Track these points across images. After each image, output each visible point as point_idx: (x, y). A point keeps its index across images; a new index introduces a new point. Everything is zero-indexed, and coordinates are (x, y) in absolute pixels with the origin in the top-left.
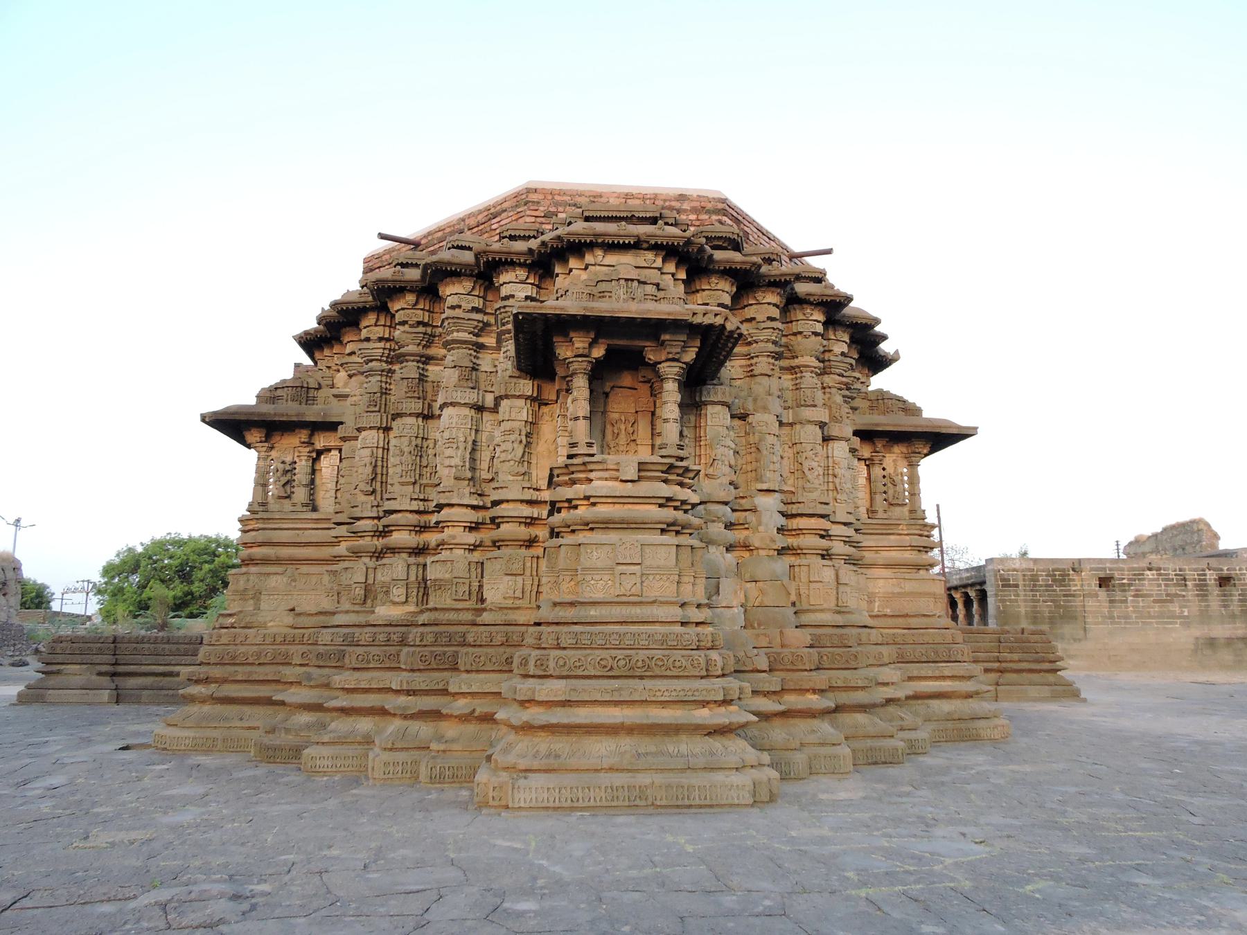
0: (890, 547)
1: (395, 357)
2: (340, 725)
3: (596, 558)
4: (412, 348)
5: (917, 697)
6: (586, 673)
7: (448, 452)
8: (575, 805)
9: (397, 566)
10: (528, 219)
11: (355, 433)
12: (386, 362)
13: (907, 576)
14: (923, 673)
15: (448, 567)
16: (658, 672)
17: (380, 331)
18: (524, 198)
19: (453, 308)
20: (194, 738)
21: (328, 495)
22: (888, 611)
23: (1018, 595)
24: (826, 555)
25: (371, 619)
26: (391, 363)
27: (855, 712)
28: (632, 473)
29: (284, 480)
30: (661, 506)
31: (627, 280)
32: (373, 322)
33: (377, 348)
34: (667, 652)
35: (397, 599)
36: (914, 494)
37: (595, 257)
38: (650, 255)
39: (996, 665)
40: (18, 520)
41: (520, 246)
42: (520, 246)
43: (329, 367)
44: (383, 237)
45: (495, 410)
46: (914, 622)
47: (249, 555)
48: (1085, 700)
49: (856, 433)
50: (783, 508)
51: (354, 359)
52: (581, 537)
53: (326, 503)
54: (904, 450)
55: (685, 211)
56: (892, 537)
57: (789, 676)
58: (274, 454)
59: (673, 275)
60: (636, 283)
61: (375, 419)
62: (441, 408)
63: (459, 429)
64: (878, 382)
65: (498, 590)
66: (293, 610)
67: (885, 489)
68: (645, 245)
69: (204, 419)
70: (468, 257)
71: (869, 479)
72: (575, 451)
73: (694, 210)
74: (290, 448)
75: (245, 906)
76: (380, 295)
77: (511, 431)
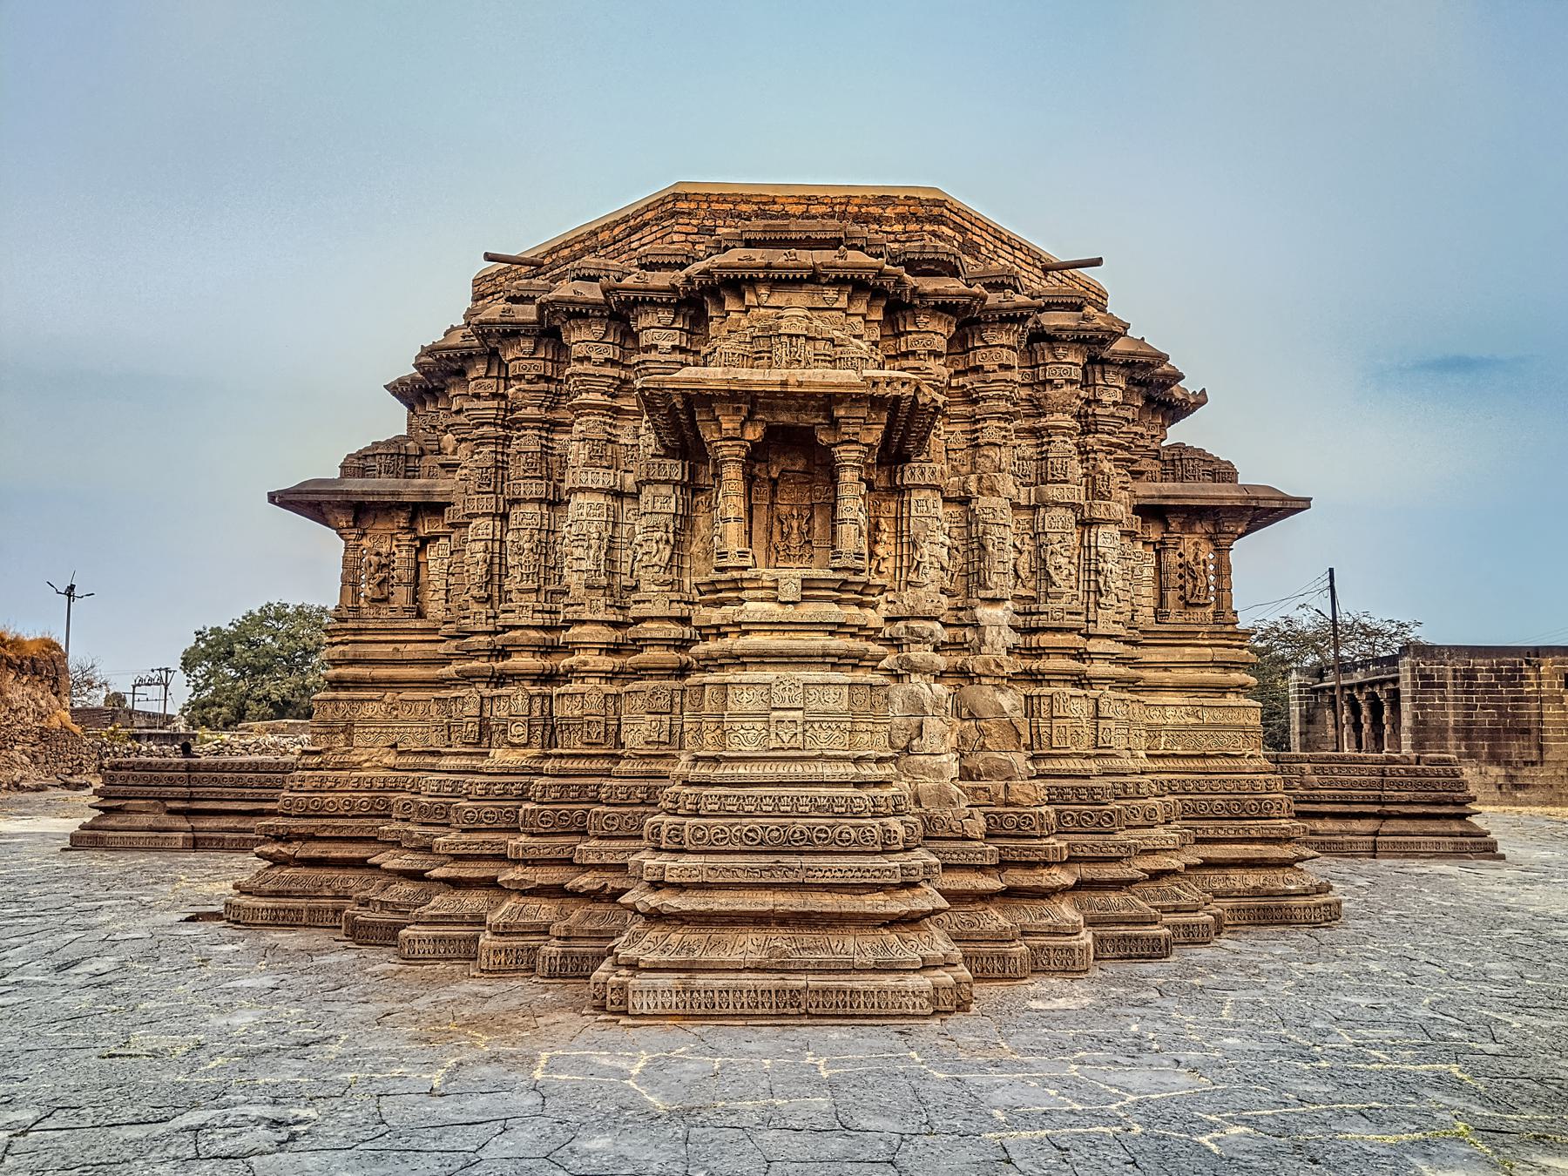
0: (1183, 665)
1: (510, 423)
2: (442, 903)
3: (744, 701)
4: (530, 412)
5: (1208, 864)
7: (578, 552)
8: (711, 1012)
9: (517, 698)
10: (676, 238)
11: (466, 520)
12: (503, 426)
13: (1205, 702)
15: (580, 700)
17: (491, 385)
18: (669, 207)
19: (580, 360)
21: (436, 597)
23: (1445, 699)
24: (1081, 680)
25: (485, 764)
26: (508, 427)
27: (1107, 889)
28: (791, 591)
29: (380, 576)
30: (831, 633)
31: (790, 336)
32: (482, 373)
33: (489, 408)
34: (831, 821)
35: (516, 740)
36: (1223, 590)
37: (758, 296)
38: (831, 293)
39: (1376, 809)
40: (72, 587)
41: (660, 279)
42: (660, 279)
43: (434, 427)
44: (489, 257)
45: (636, 496)
47: (337, 676)
48: (1502, 857)
49: (1137, 510)
50: (1020, 621)
51: (462, 418)
52: (730, 676)
53: (435, 608)
55: (888, 219)
56: (1188, 650)
57: (1011, 843)
58: (366, 542)
59: (864, 316)
60: (802, 340)
61: (487, 503)
62: (572, 491)
63: (591, 522)
64: (1178, 433)
65: (639, 732)
66: (394, 746)
68: (824, 280)
69: (272, 498)
70: (593, 293)
71: (1159, 570)
72: (723, 563)
73: (902, 218)
74: (387, 541)
75: (284, 1135)
76: (487, 343)
77: (655, 527)
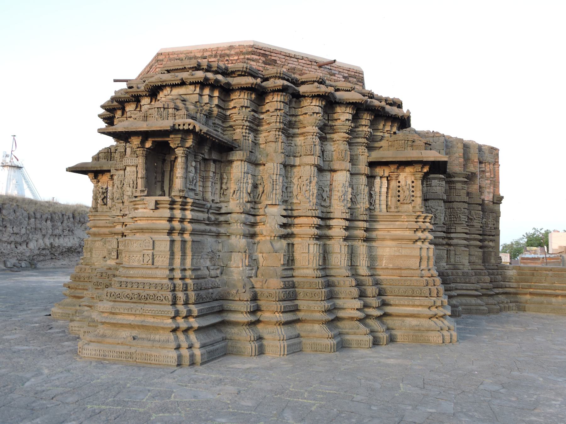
6: (122, 300)
14: (402, 302)
16: (151, 301)
20: (62, 313)
22: (391, 266)
29: (103, 196)
35: (113, 257)
38: (192, 88)
46: (404, 273)
50: (285, 213)
54: (412, 170)
55: (232, 55)
67: (398, 194)
73: (237, 54)
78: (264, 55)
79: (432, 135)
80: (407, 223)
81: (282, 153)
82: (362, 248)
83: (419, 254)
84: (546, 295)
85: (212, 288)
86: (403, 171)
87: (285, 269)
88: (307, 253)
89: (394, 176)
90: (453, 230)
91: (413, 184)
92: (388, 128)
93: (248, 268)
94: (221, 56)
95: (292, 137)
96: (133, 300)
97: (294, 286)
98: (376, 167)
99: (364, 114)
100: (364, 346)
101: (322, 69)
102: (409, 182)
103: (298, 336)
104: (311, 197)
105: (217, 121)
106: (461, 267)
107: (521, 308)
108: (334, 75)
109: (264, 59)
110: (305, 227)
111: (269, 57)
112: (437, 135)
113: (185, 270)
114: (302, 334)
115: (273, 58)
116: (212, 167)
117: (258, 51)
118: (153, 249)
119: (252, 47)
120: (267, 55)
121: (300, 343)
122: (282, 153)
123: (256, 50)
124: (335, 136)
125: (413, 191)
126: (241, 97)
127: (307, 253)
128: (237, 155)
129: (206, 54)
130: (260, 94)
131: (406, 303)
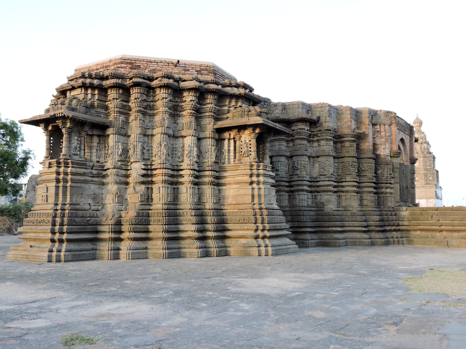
22: (234, 202)
38: (79, 90)
46: (241, 207)
73: (114, 65)
78: (130, 63)
79: (320, 106)
80: (244, 171)
81: (140, 127)
82: (208, 190)
83: (251, 193)
84: (432, 230)
85: (89, 217)
86: (243, 133)
87: (142, 204)
88: (160, 194)
89: (237, 137)
90: (343, 180)
91: (250, 143)
92: (233, 103)
93: (118, 204)
94: (106, 67)
95: (154, 116)
96: (35, 224)
97: (148, 215)
98: (225, 132)
99: (208, 95)
100: (194, 256)
101: (177, 67)
102: (247, 141)
103: (146, 248)
104: (162, 155)
105: (99, 110)
106: (350, 209)
107: (410, 242)
108: (188, 70)
109: (130, 66)
110: (159, 177)
111: (135, 64)
112: (324, 105)
113: (65, 204)
114: (149, 247)
115: (137, 64)
116: (96, 140)
117: (126, 61)
118: (47, 192)
119: (121, 59)
120: (132, 63)
121: (147, 252)
122: (140, 127)
123: (124, 61)
124: (184, 113)
125: (250, 148)
126: (112, 92)
127: (160, 194)
128: (110, 131)
129: (98, 67)
130: (126, 90)
131: (239, 228)
